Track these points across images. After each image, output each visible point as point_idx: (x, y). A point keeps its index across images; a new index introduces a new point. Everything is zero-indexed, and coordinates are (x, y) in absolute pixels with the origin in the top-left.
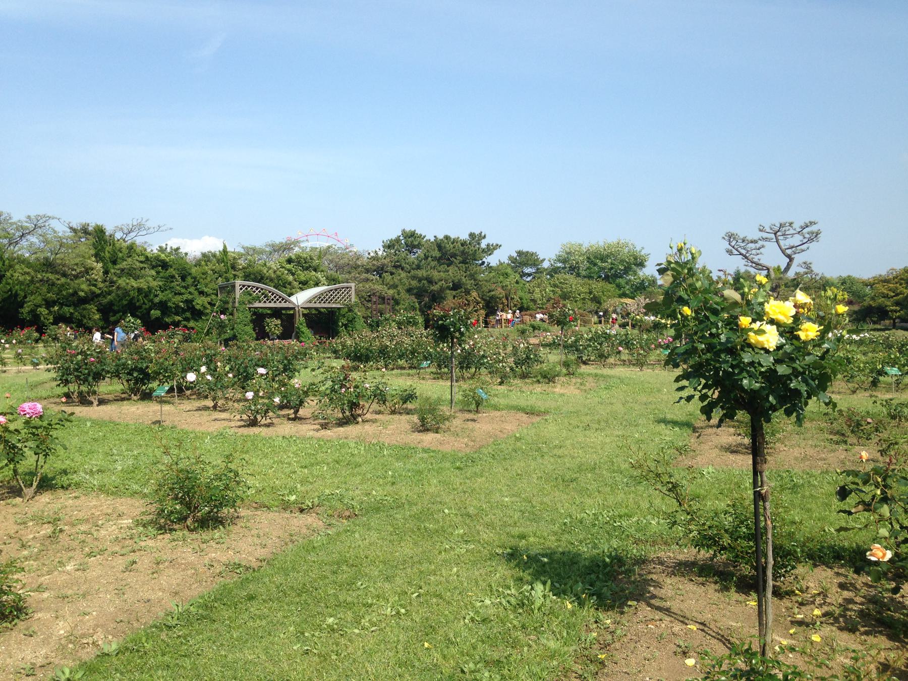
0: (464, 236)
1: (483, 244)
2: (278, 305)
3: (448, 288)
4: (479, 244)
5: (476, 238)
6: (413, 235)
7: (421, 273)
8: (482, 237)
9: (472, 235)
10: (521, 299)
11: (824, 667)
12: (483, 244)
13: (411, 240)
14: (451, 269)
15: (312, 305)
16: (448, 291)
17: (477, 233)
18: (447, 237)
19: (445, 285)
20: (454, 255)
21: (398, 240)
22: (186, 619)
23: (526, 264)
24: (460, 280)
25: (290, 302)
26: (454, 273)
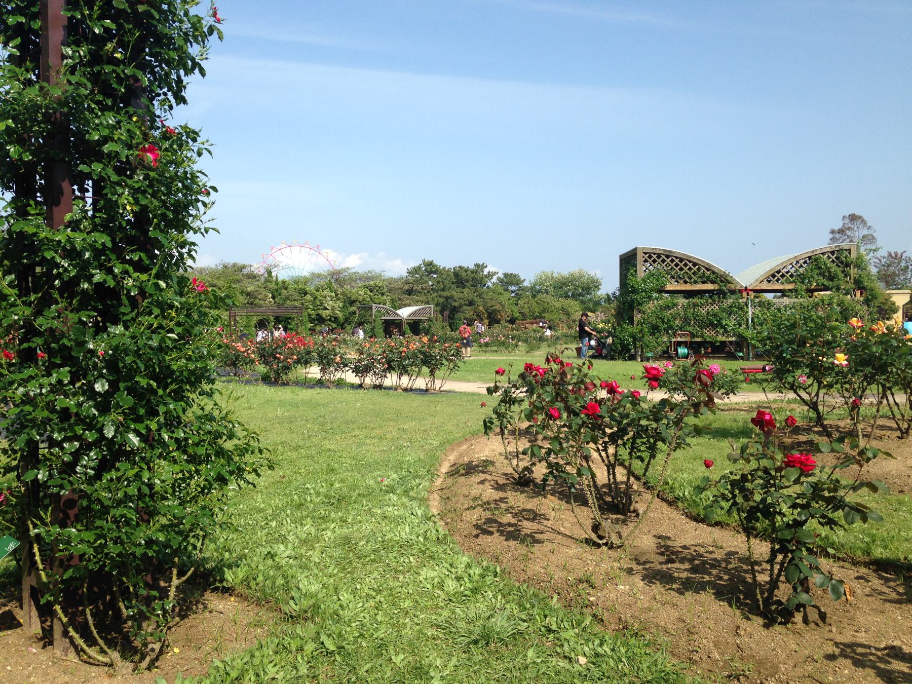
0: (472, 267)
1: (486, 272)
2: (393, 318)
3: (466, 305)
4: (482, 272)
5: (480, 267)
6: (431, 264)
7: (445, 294)
8: (484, 266)
9: (477, 265)
10: (512, 311)
11: (331, 638)
12: (486, 272)
13: (430, 268)
14: (466, 291)
15: (411, 318)
16: (465, 307)
17: (481, 263)
18: (460, 267)
19: (463, 303)
20: (467, 281)
21: (419, 267)
22: (679, 390)
23: (511, 284)
24: (472, 299)
25: (398, 315)
26: (467, 293)
